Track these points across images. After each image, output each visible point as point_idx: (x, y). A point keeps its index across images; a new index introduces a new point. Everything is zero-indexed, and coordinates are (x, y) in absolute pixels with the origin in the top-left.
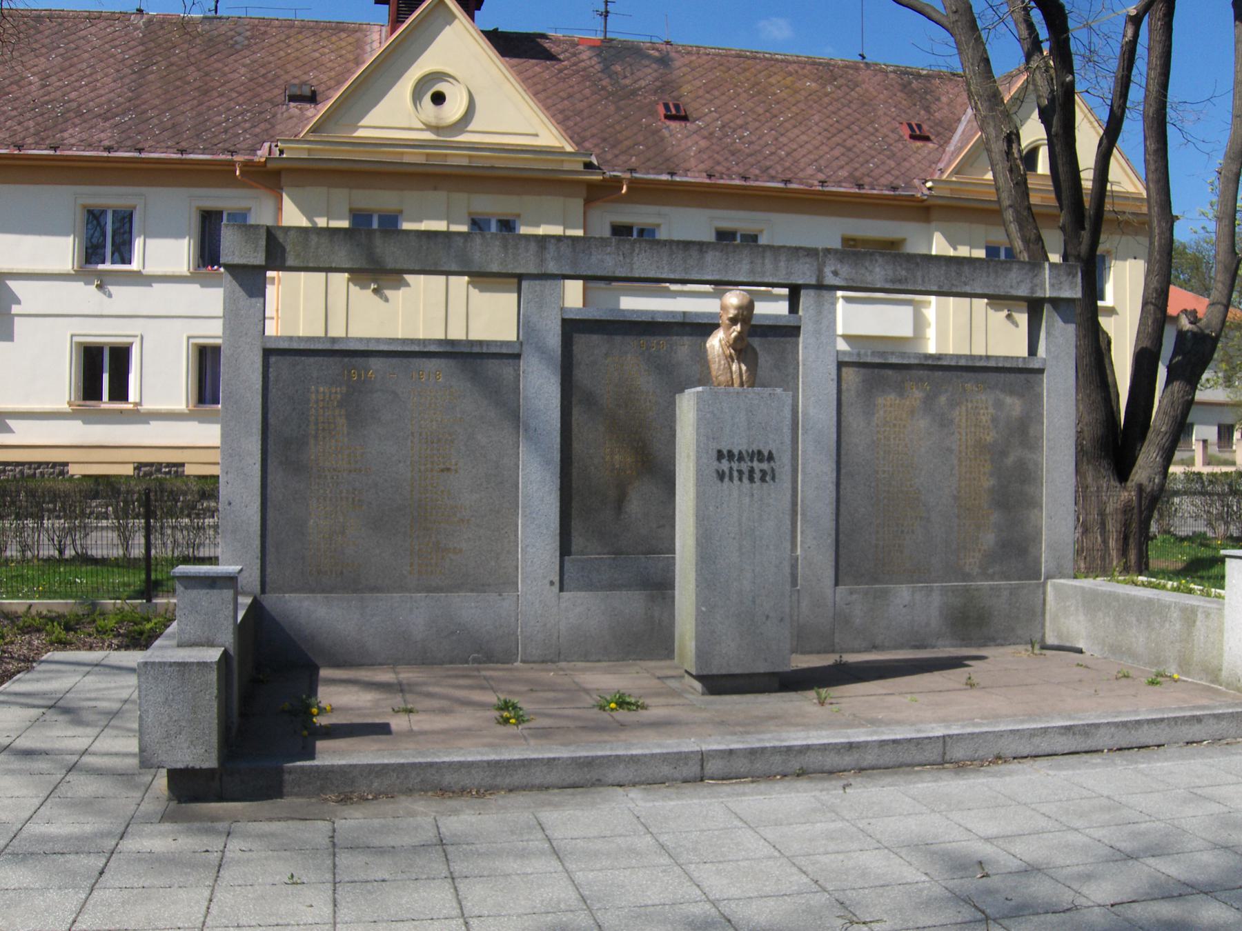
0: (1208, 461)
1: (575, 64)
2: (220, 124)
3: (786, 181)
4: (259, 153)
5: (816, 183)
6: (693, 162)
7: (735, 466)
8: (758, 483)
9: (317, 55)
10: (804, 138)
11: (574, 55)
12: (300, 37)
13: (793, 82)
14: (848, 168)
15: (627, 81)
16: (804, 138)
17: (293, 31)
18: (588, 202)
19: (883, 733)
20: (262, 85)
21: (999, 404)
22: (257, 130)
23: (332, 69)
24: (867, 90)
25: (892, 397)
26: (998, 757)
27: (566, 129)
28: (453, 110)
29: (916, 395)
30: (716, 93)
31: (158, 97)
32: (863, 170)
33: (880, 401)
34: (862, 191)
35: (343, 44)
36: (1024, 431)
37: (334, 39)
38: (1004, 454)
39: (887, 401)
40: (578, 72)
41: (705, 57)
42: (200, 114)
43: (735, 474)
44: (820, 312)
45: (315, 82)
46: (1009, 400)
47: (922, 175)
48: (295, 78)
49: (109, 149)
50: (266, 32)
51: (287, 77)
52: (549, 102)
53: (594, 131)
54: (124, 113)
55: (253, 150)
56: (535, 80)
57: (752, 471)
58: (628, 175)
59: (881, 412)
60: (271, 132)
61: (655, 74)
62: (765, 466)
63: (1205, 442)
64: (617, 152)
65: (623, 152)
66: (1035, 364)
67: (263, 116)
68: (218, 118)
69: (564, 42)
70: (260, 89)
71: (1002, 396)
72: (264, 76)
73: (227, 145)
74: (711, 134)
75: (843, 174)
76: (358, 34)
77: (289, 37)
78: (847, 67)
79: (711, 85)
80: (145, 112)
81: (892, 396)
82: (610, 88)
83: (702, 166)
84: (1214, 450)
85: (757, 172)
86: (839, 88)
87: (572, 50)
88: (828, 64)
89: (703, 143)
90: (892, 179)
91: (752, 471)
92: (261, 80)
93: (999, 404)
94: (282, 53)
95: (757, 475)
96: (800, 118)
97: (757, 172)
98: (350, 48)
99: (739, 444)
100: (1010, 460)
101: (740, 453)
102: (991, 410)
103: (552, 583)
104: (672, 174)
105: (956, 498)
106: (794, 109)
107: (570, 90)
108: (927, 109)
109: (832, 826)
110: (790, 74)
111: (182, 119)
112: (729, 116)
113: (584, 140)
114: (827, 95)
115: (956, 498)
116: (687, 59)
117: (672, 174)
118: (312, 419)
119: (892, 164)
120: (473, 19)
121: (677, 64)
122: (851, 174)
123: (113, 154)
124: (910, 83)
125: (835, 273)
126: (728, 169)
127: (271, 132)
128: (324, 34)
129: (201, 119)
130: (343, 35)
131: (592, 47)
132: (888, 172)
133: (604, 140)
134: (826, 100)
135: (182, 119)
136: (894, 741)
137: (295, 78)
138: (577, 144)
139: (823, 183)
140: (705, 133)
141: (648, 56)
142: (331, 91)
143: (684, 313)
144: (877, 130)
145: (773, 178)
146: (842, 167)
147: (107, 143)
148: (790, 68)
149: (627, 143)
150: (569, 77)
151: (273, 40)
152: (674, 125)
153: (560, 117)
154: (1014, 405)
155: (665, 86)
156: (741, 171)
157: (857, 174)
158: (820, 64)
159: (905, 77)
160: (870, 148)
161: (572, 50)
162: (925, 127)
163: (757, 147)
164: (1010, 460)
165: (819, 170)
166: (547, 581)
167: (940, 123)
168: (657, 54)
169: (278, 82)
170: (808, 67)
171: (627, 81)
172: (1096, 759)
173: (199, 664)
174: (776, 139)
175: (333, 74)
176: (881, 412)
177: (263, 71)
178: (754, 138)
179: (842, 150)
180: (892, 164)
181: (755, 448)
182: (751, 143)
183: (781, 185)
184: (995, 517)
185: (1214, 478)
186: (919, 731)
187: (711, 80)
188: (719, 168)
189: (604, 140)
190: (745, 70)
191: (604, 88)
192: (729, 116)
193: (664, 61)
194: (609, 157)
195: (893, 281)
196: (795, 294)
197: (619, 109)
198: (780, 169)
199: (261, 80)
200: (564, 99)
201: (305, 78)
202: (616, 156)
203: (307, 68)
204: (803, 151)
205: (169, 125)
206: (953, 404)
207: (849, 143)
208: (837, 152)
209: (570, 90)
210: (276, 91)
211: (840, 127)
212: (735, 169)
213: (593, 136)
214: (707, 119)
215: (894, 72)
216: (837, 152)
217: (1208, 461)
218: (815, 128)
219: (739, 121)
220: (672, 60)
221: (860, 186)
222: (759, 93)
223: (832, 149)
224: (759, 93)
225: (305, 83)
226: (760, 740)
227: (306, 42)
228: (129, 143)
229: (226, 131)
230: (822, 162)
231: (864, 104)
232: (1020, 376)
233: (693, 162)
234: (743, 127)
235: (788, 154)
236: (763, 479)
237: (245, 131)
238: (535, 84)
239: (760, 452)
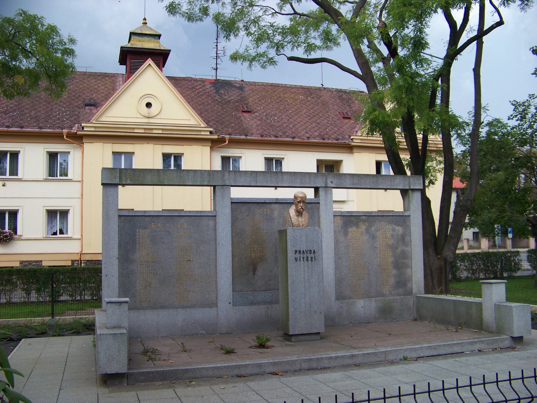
0: (470, 247)
1: (204, 90)
2: (56, 116)
3: (293, 138)
4: (73, 128)
5: (305, 138)
6: (255, 130)
7: (302, 256)
8: (310, 262)
9: (96, 87)
10: (300, 119)
11: (204, 86)
12: (89, 79)
13: (294, 96)
14: (318, 131)
15: (226, 97)
16: (300, 119)
17: (85, 77)
18: (211, 148)
19: (363, 351)
20: (73, 100)
21: (393, 230)
22: (72, 119)
23: (103, 93)
24: (325, 99)
25: (354, 229)
26: (405, 359)
27: (202, 117)
28: (154, 110)
29: (363, 227)
30: (263, 101)
31: (29, 104)
32: (325, 132)
33: (350, 230)
34: (325, 141)
35: (107, 82)
36: (404, 239)
37: (103, 80)
38: (396, 248)
39: (352, 230)
40: (205, 93)
41: (257, 86)
42: (47, 112)
43: (302, 259)
44: (326, 197)
45: (96, 99)
46: (397, 228)
47: (349, 134)
48: (87, 96)
49: (8, 127)
50: (74, 77)
51: (84, 96)
52: (194, 106)
53: (213, 118)
54: (14, 111)
55: (71, 128)
56: (188, 97)
57: (307, 258)
58: (228, 136)
59: (350, 234)
60: (78, 120)
61: (237, 94)
62: (312, 255)
63: (468, 240)
64: (223, 126)
65: (226, 127)
66: (407, 214)
67: (74, 113)
68: (55, 114)
69: (200, 81)
70: (73, 101)
71: (394, 226)
72: (74, 96)
73: (60, 125)
74: (262, 118)
75: (316, 134)
76: (113, 78)
77: (84, 79)
78: (316, 89)
79: (261, 98)
80: (23, 111)
81: (354, 228)
82: (219, 100)
83: (258, 132)
84: (471, 243)
85: (281, 134)
86: (313, 98)
87: (202, 84)
88: (308, 88)
89: (258, 122)
90: (336, 135)
91: (307, 258)
92: (74, 98)
93: (393, 230)
94: (81, 86)
95: (310, 259)
96: (298, 111)
97: (281, 134)
98: (110, 84)
99: (303, 248)
100: (399, 251)
101: (303, 251)
102: (391, 232)
103: (230, 303)
104: (246, 136)
105: (379, 266)
106: (295, 107)
107: (203, 101)
108: (350, 106)
109: (352, 382)
110: (293, 93)
111: (39, 114)
112: (269, 111)
113: (210, 121)
114: (308, 101)
115: (379, 266)
116: (250, 87)
117: (246, 136)
118: (137, 242)
119: (336, 129)
120: (162, 71)
121: (246, 89)
122: (320, 134)
123: (10, 129)
124: (342, 96)
125: (332, 182)
126: (269, 133)
127: (78, 120)
128: (99, 78)
129: (48, 114)
130: (107, 78)
131: (211, 83)
132: (335, 133)
133: (218, 122)
134: (308, 103)
135: (39, 114)
136: (368, 354)
137: (87, 96)
138: (207, 124)
139: (308, 138)
140: (259, 118)
141: (235, 87)
142: (103, 103)
143: (277, 199)
144: (329, 115)
145: (287, 137)
146: (316, 131)
147: (7, 124)
148: (293, 90)
149: (227, 123)
150: (202, 95)
151: (78, 81)
152: (245, 115)
153: (199, 112)
154: (399, 230)
155: (242, 99)
156: (274, 134)
157: (322, 134)
158: (305, 88)
159: (340, 93)
160: (327, 123)
161: (202, 84)
162: (349, 114)
163: (280, 124)
164: (399, 251)
165: (307, 133)
166: (228, 302)
167: (355, 112)
168: (238, 85)
169: (80, 98)
170: (300, 90)
171: (226, 97)
172: (440, 358)
173: (120, 334)
174: (288, 120)
175: (103, 95)
176: (350, 234)
177: (73, 94)
178: (279, 120)
179: (316, 124)
180: (336, 129)
181: (309, 249)
182: (278, 122)
183: (291, 139)
184: (394, 272)
185: (474, 255)
186: (376, 350)
187: (261, 96)
188: (265, 132)
189: (218, 122)
190: (274, 92)
191: (216, 100)
192: (269, 111)
193: (241, 88)
194: (220, 129)
195: (353, 185)
196: (317, 190)
197: (223, 108)
198: (290, 132)
199: (74, 98)
200: (200, 105)
201: (92, 97)
202: (223, 128)
203: (92, 92)
204: (299, 125)
205: (34, 116)
206: (377, 230)
207: (318, 121)
208: (313, 125)
209: (203, 101)
210: (80, 102)
211: (314, 114)
212: (272, 133)
213: (213, 120)
214: (260, 112)
215: (336, 91)
216: (313, 125)
217: (470, 247)
218: (304, 115)
219: (273, 113)
220: (244, 88)
221: (324, 139)
222: (281, 101)
223: (311, 124)
224: (281, 101)
225: (91, 99)
226: (320, 355)
227: (91, 81)
228: (16, 124)
229: (59, 119)
230: (308, 129)
231: (324, 105)
232: (399, 219)
233: (255, 130)
234: (275, 115)
235: (293, 126)
236: (312, 261)
237: (67, 119)
238: (188, 99)
239: (310, 251)
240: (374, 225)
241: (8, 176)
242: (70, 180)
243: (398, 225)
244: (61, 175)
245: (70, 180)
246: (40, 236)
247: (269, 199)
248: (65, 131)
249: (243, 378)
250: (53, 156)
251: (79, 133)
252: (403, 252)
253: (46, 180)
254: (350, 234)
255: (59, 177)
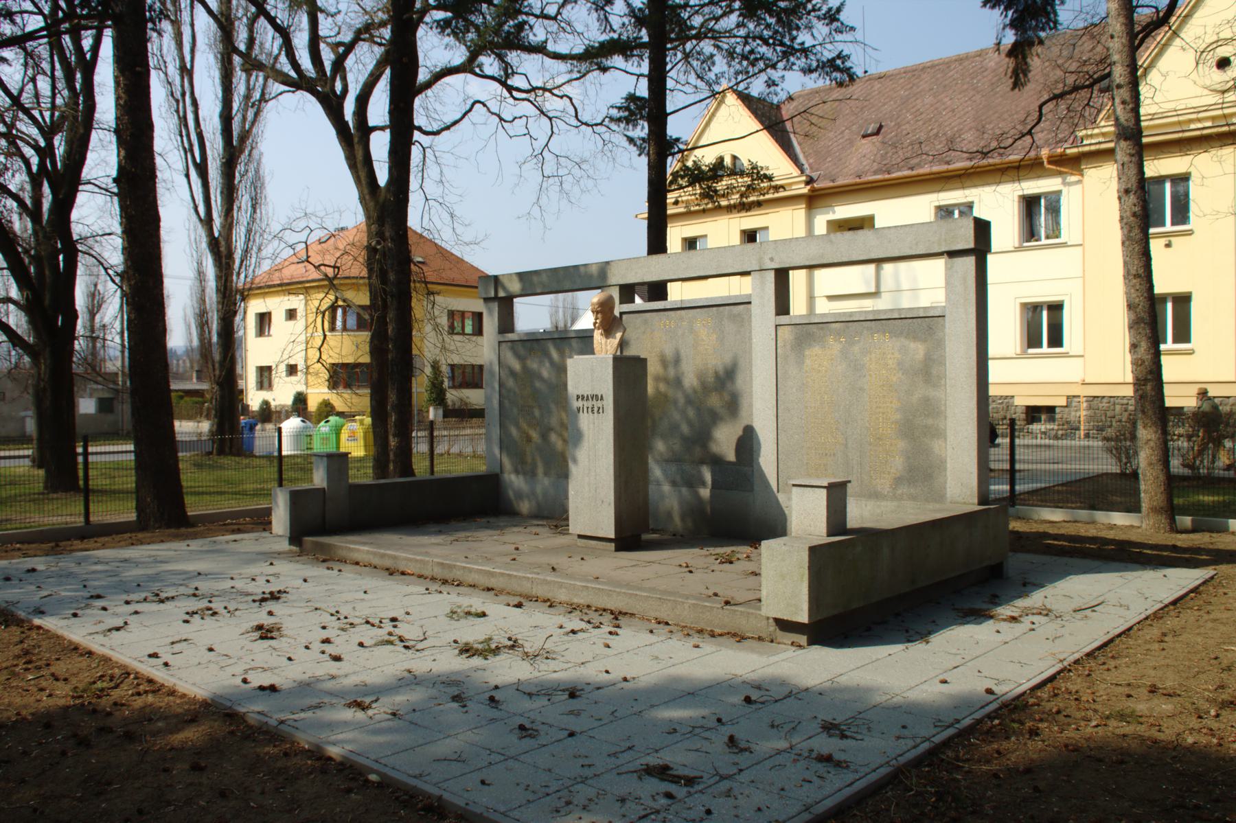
36: (929, 371)
39: (814, 353)
46: (912, 345)
71: (907, 342)
102: (897, 355)
154: (918, 350)
184: (902, 444)
240: (859, 341)
241: (1168, 227)
242: (1064, 245)
243: (916, 339)
244: (1047, 237)
245: (1064, 245)
246: (1011, 354)
247: (689, 301)
248: (1045, 153)
249: (397, 577)
250: (1030, 204)
251: (1068, 151)
252: (926, 400)
253: (1019, 249)
254: (808, 362)
255: (1044, 241)
